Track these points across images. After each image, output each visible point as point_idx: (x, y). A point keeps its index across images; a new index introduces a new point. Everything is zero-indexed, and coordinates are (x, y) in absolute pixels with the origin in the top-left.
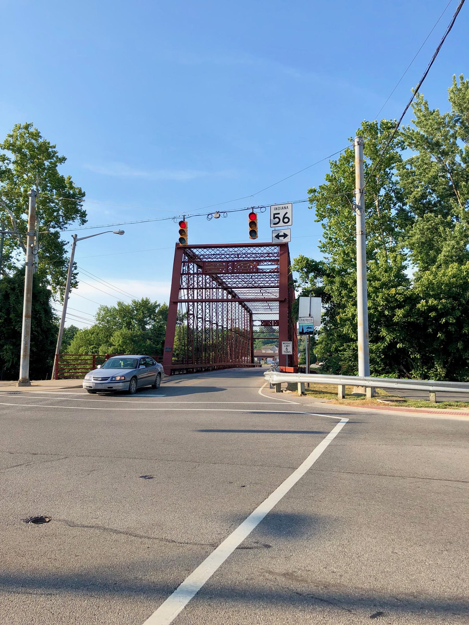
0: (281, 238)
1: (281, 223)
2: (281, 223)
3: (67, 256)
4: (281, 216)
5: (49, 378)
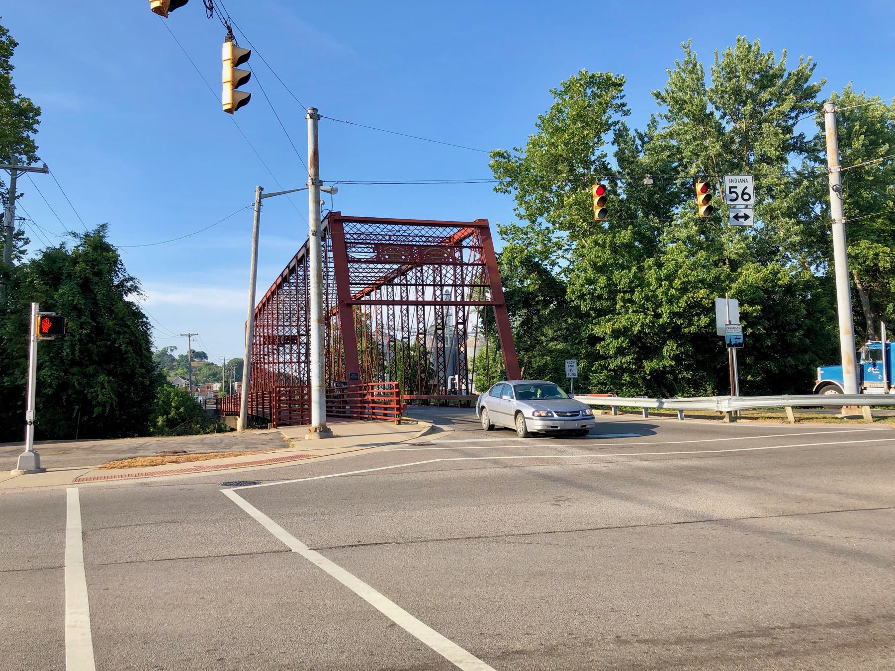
0: (742, 220)
1: (740, 200)
2: (740, 200)
3: (480, 320)
4: (739, 191)
5: (730, 394)
